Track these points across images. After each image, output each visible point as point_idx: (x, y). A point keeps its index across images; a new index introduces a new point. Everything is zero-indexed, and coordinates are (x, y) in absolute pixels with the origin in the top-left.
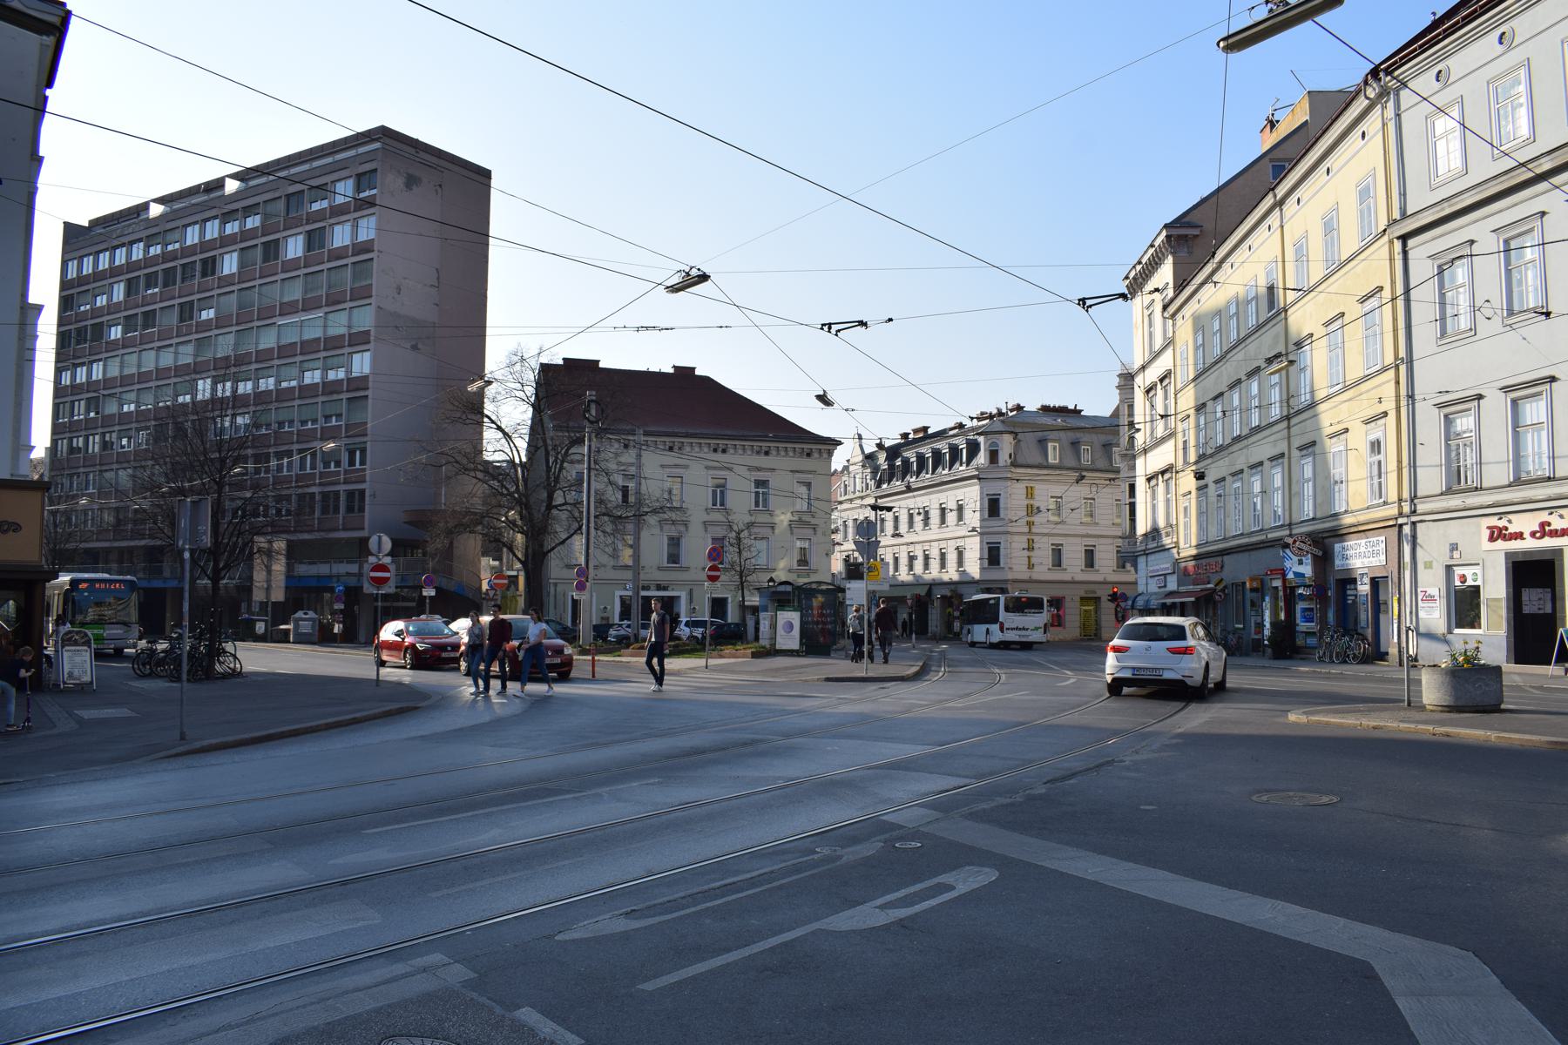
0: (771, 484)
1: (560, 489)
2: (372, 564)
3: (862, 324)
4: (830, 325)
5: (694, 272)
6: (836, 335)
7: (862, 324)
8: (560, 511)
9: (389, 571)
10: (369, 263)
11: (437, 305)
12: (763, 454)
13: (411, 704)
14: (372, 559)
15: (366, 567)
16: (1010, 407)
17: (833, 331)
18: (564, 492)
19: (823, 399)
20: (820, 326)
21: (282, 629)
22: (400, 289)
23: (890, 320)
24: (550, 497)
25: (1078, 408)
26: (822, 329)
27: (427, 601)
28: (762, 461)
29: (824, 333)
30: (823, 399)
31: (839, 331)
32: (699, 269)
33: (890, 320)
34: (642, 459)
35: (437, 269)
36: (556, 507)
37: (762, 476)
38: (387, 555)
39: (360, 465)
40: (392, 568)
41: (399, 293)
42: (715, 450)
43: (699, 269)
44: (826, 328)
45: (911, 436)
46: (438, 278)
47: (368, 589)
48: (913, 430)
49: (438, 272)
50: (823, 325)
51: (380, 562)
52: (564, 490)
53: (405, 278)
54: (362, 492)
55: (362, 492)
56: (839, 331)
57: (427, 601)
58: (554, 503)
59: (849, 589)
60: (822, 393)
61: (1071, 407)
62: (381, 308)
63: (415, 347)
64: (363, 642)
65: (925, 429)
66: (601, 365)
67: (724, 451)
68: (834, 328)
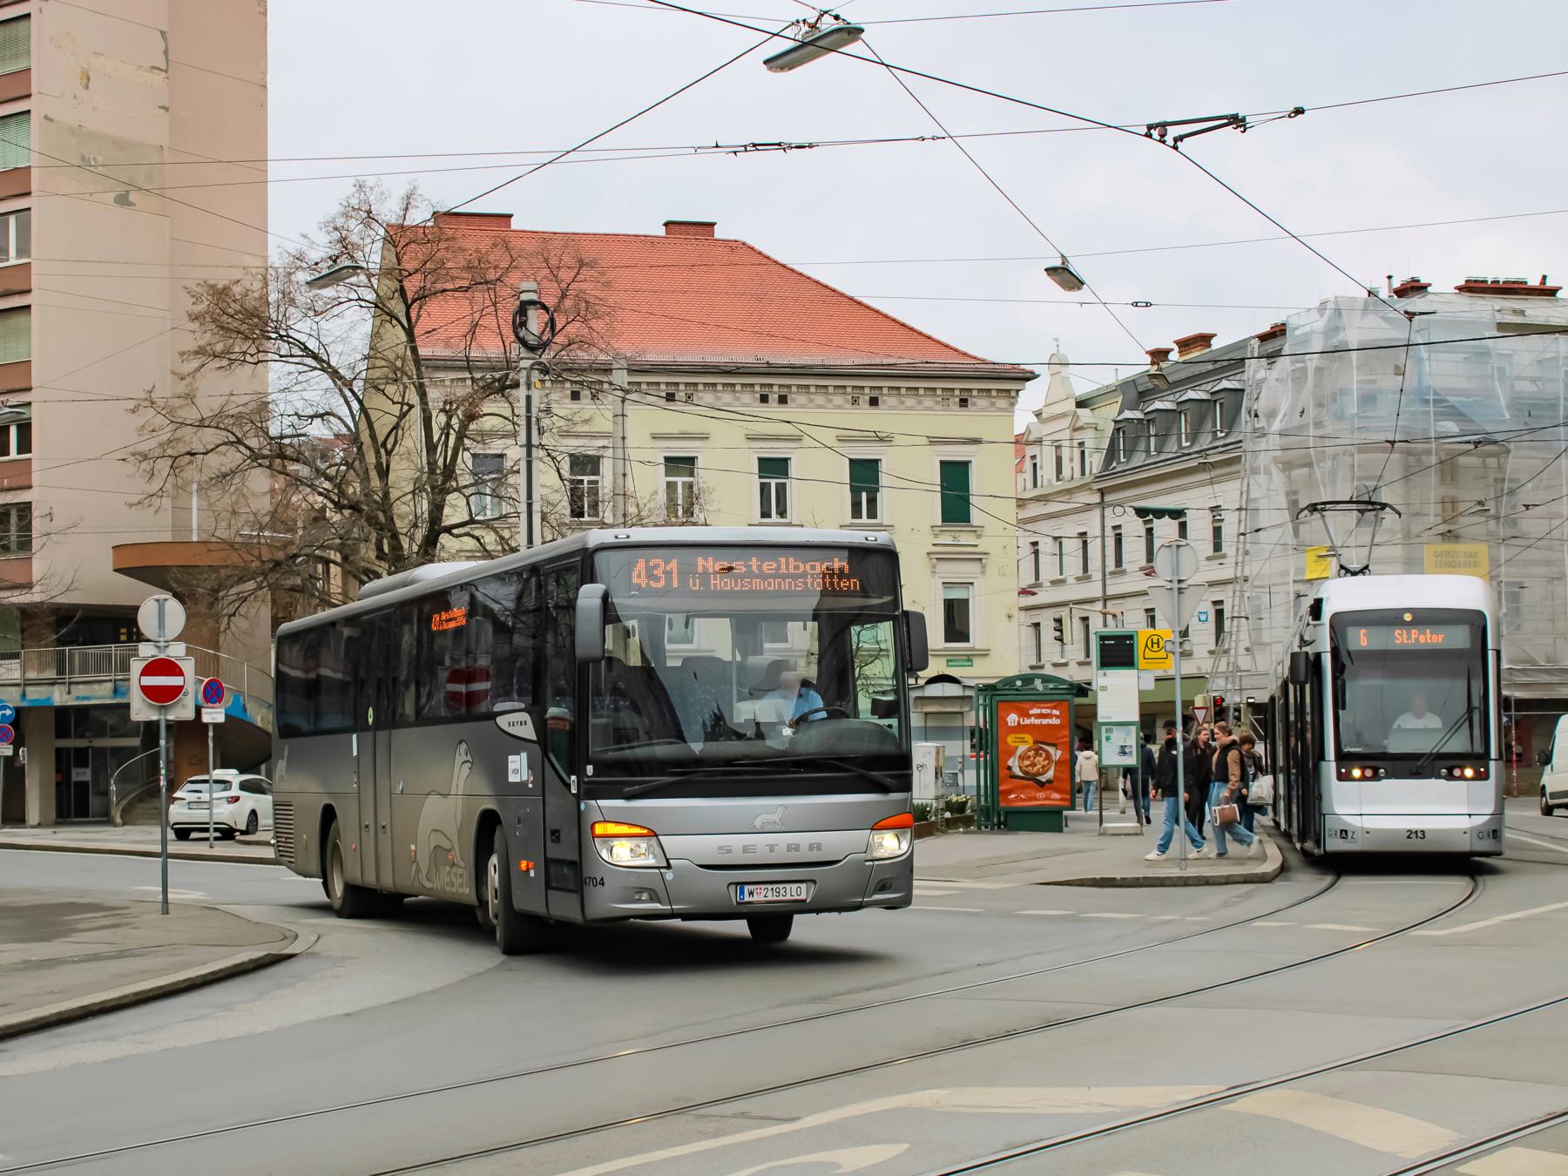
0: (793, 469)
1: (458, 489)
2: (144, 659)
3: (1237, 121)
4: (1163, 126)
5: (828, 24)
6: (1175, 147)
7: (1237, 121)
8: (457, 536)
9: (181, 673)
10: (22, 25)
11: (166, 109)
12: (775, 404)
13: (274, 949)
14: (146, 651)
15: (137, 667)
16: (1396, 284)
17: (1169, 139)
18: (467, 498)
19: (1064, 276)
20: (1145, 130)
21: (1216, 770)
22: (88, 79)
23: (1299, 111)
24: (437, 509)
25: (1550, 284)
26: (1149, 136)
27: (211, 734)
28: (865, 418)
29: (1152, 145)
30: (1064, 276)
31: (1181, 138)
32: (837, 17)
33: (1299, 111)
34: (628, 421)
35: (162, 33)
36: (448, 530)
37: (680, 449)
38: (178, 639)
39: (19, 452)
40: (188, 666)
41: (87, 87)
42: (764, 399)
43: (837, 17)
44: (1155, 133)
45: (1174, 356)
46: (166, 52)
47: (141, 710)
48: (1179, 343)
49: (165, 39)
50: (1150, 127)
51: (162, 656)
52: (467, 492)
53: (98, 54)
54: (28, 505)
55: (28, 505)
56: (1181, 138)
57: (211, 734)
58: (446, 522)
59: (1104, 689)
60: (1058, 263)
61: (1534, 282)
62: (51, 120)
63: (123, 200)
64: (36, 822)
65: (1204, 340)
66: (719, 233)
67: (783, 400)
68: (1173, 132)
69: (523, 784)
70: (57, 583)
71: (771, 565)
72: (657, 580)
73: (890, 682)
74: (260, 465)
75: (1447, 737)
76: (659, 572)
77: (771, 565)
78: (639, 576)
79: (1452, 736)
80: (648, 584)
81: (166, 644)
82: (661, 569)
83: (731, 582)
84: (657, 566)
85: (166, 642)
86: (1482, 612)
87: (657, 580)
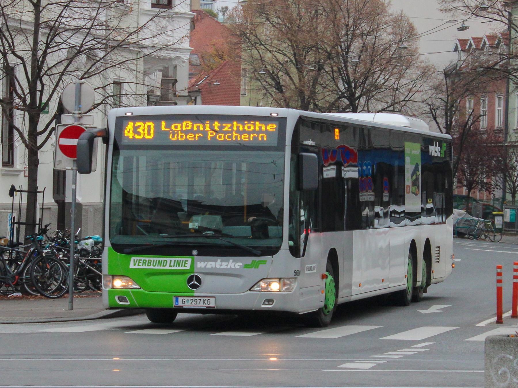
51: (76, 124)
69: (444, 143)
70: (403, 105)
71: (273, 126)
72: (139, 134)
73: (514, 51)
74: (334, 93)
75: (423, 35)
76: (140, 130)
77: (273, 126)
78: (129, 132)
79: (499, 290)
80: (133, 137)
81: (79, 115)
82: (142, 128)
83: (192, 138)
84: (139, 126)
85: (79, 114)
86: (295, 257)
87: (139, 134)
